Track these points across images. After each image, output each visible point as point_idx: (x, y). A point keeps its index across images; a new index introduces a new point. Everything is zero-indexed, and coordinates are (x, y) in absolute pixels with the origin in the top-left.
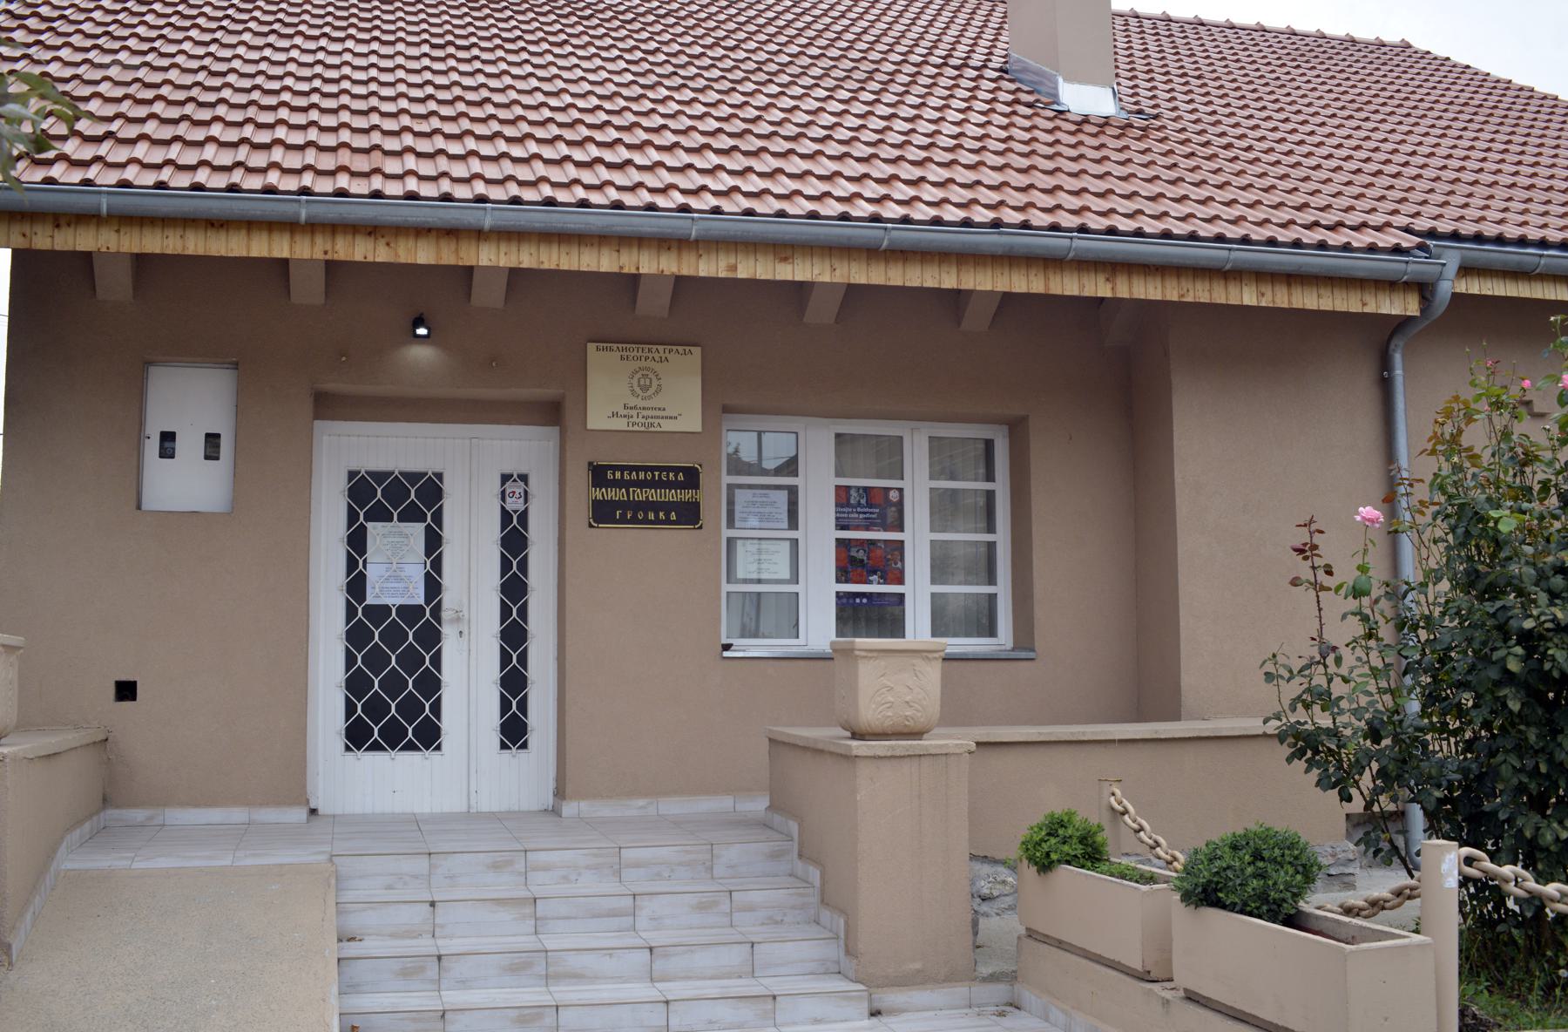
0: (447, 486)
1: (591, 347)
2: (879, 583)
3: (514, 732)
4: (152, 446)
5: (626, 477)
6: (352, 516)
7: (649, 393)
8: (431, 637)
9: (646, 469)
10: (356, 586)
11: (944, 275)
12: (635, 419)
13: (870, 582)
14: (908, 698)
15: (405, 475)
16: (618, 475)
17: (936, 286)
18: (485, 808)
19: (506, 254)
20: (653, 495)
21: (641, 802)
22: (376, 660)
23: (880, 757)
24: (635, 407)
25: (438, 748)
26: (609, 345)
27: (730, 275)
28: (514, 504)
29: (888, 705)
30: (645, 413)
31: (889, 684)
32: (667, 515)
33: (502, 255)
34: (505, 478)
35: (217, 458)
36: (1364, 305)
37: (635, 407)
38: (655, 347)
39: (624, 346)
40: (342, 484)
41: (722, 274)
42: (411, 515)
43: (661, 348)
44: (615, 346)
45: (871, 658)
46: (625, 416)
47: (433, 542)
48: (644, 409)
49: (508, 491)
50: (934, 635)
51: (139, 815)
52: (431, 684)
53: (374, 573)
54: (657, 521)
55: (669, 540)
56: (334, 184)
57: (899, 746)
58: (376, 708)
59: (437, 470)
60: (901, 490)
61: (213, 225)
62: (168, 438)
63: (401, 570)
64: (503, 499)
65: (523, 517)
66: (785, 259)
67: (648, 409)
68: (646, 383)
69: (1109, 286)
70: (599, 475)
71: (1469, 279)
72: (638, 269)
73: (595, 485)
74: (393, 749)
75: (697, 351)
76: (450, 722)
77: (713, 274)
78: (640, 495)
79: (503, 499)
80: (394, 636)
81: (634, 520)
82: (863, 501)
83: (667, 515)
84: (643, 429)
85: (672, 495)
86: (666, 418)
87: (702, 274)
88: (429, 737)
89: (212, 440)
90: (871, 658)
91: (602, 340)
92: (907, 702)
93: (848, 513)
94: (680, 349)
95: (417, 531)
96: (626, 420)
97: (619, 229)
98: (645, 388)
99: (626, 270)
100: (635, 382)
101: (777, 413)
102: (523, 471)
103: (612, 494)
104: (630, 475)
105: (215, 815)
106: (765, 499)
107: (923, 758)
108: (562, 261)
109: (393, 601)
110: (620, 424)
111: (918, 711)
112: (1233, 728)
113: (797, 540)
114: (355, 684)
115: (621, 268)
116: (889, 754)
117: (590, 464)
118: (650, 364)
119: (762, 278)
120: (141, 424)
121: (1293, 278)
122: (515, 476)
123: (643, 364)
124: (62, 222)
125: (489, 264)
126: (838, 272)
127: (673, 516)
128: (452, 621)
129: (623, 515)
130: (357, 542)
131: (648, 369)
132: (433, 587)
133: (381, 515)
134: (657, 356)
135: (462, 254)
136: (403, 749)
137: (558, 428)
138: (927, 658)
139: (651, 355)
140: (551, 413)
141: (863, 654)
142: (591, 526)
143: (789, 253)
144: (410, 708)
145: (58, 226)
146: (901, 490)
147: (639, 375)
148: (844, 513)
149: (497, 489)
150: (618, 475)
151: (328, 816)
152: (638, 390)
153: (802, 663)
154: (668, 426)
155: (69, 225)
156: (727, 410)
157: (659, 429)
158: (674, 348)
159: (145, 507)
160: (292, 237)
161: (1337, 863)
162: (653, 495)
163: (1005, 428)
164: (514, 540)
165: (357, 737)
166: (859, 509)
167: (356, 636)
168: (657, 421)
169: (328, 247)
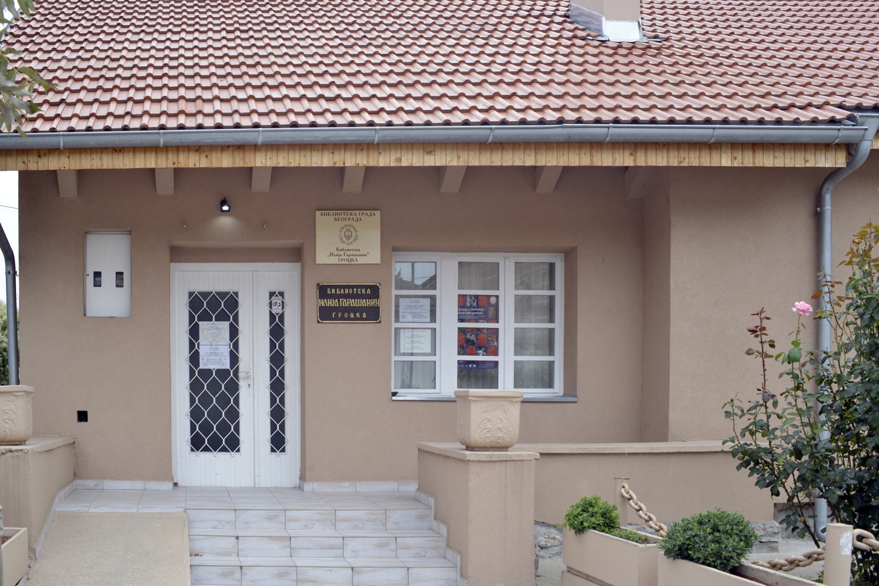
0: (240, 300)
1: (318, 213)
2: (483, 355)
3: (278, 442)
4: (90, 280)
5: (338, 292)
6: (191, 318)
8: (234, 387)
10: (194, 358)
11: (527, 158)
12: (343, 257)
13: (478, 354)
14: (500, 426)
15: (218, 293)
16: (333, 291)
17: (522, 164)
19: (270, 158)
20: (353, 303)
21: (347, 484)
22: (206, 400)
23: (483, 462)
24: (343, 250)
25: (238, 451)
26: (327, 212)
27: (398, 165)
28: (277, 310)
29: (488, 430)
30: (349, 253)
31: (489, 417)
32: (361, 315)
34: (272, 294)
35: (122, 286)
36: (806, 161)
37: (343, 250)
38: (354, 212)
40: (186, 300)
41: (393, 164)
42: (222, 317)
43: (357, 212)
44: (331, 212)
45: (479, 401)
46: (337, 255)
47: (234, 332)
48: (348, 250)
51: (91, 483)
52: (234, 415)
53: (203, 351)
54: (355, 319)
60: (497, 297)
61: (116, 150)
62: (97, 275)
63: (217, 349)
66: (430, 153)
67: (350, 250)
69: (632, 158)
70: (323, 291)
72: (344, 163)
75: (378, 213)
77: (387, 165)
78: (345, 303)
79: (271, 307)
81: (343, 318)
83: (361, 315)
84: (347, 263)
85: (364, 303)
86: (360, 255)
87: (381, 165)
88: (234, 444)
90: (479, 401)
92: (499, 428)
94: (368, 212)
95: (225, 326)
96: (337, 257)
99: (337, 165)
100: (342, 234)
102: (281, 290)
103: (331, 303)
104: (340, 291)
105: (127, 485)
107: (507, 462)
108: (301, 161)
110: (334, 260)
111: (505, 434)
112: (586, 449)
113: (435, 329)
114: (195, 414)
117: (318, 285)
118: (351, 222)
120: (84, 268)
121: (756, 146)
122: (277, 293)
123: (347, 223)
124: (42, 154)
125: (261, 165)
127: (364, 315)
128: (244, 378)
129: (337, 315)
130: (194, 333)
131: (349, 226)
132: (234, 359)
133: (206, 317)
134: (355, 218)
135: (247, 160)
136: (203, 450)
139: (351, 217)
141: (474, 399)
142: (319, 322)
143: (432, 148)
144: (224, 428)
145: (40, 156)
146: (497, 297)
149: (267, 301)
150: (333, 291)
154: (361, 260)
156: (395, 249)
157: (356, 262)
158: (365, 212)
159: (87, 315)
162: (353, 303)
163: (562, 255)
164: (277, 331)
165: (197, 444)
166: (472, 309)
167: (195, 387)
169: (175, 160)
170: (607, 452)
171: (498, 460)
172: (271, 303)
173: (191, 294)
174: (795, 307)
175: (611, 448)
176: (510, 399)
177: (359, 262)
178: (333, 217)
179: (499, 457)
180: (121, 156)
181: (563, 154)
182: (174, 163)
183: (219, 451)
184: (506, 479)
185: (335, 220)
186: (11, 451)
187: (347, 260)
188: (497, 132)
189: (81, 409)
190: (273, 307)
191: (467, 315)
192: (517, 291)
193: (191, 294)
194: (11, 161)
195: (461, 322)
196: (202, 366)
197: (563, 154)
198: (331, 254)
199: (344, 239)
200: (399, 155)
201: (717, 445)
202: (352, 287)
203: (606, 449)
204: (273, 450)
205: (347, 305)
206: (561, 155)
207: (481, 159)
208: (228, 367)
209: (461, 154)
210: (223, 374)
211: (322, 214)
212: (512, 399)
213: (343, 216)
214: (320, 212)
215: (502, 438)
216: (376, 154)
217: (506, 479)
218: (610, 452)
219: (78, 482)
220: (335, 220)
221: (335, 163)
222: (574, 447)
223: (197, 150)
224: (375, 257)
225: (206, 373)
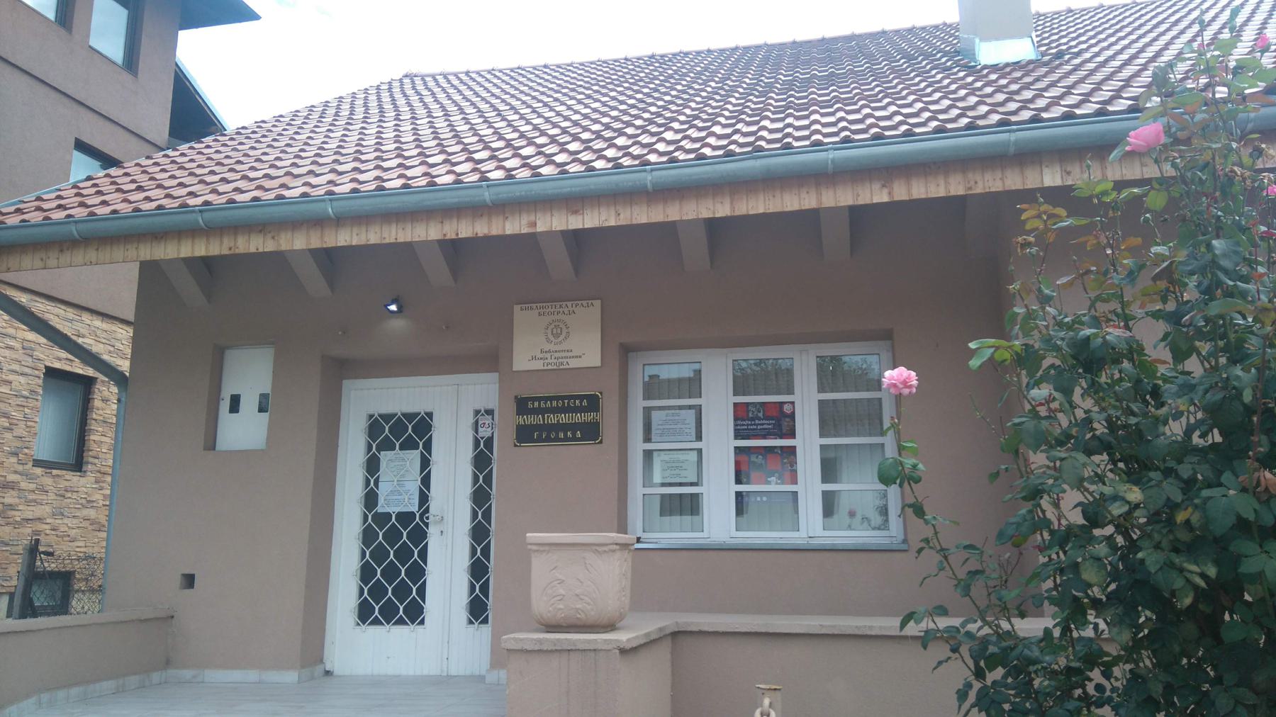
0: (436, 422)
1: (517, 308)
2: (777, 484)
3: (477, 610)
4: (225, 405)
5: (543, 405)
6: (370, 448)
7: (560, 339)
8: (419, 535)
10: (370, 499)
11: (719, 206)
12: (549, 361)
13: (769, 483)
14: (578, 591)
17: (711, 216)
19: (357, 235)
20: (564, 418)
22: (380, 555)
23: (527, 651)
24: (549, 351)
25: (422, 622)
26: (529, 305)
27: (531, 230)
29: (559, 598)
30: (557, 355)
31: (560, 577)
32: (574, 434)
33: (355, 236)
34: (477, 412)
37: (549, 351)
38: (564, 303)
39: (541, 304)
40: (363, 424)
41: (525, 230)
42: (409, 445)
43: (569, 304)
44: (534, 305)
45: (544, 551)
46: (541, 359)
47: (425, 463)
48: (556, 351)
49: (480, 422)
51: (187, 674)
52: (418, 573)
53: (383, 491)
54: (566, 439)
55: (582, 452)
56: (473, 229)
57: (547, 640)
60: (793, 403)
61: (156, 238)
63: (403, 486)
64: (477, 431)
66: (575, 212)
67: (559, 351)
68: (557, 331)
69: (885, 191)
70: (522, 405)
72: (457, 234)
74: (413, 623)
75: (598, 303)
77: (516, 231)
78: (553, 419)
79: (477, 431)
80: (393, 536)
81: (548, 439)
82: (761, 415)
83: (574, 434)
84: (555, 367)
85: (579, 418)
86: (573, 357)
87: (508, 232)
88: (415, 614)
90: (544, 551)
91: (526, 301)
92: (577, 595)
93: (748, 425)
94: (584, 303)
95: (414, 456)
96: (542, 361)
97: (429, 203)
98: (557, 336)
99: (448, 237)
100: (549, 331)
101: (689, 347)
102: (472, 414)
104: (545, 404)
105: (236, 675)
106: (677, 418)
107: (571, 653)
108: (399, 235)
109: (394, 509)
110: (538, 365)
111: (589, 604)
112: (834, 627)
113: (701, 449)
114: (366, 573)
115: (445, 235)
116: (537, 648)
117: (516, 397)
118: (560, 317)
119: (558, 229)
122: (483, 411)
123: (556, 317)
125: (345, 244)
126: (622, 216)
128: (436, 523)
129: (540, 436)
130: (372, 466)
131: (559, 321)
132: (424, 499)
133: (387, 445)
135: (326, 239)
136: (372, 623)
137: (496, 375)
138: (599, 552)
139: (561, 310)
141: (534, 548)
142: (516, 446)
145: (62, 251)
146: (793, 403)
147: (552, 326)
148: (743, 425)
149: (471, 420)
151: (340, 676)
152: (552, 338)
153: (685, 553)
154: (574, 364)
155: (68, 250)
157: (567, 367)
158: (580, 302)
160: (208, 240)
162: (564, 418)
165: (364, 614)
166: (757, 422)
167: (368, 536)
168: (565, 360)
169: (232, 244)
170: (873, 633)
171: (554, 648)
172: (477, 422)
174: (1021, 370)
175: (881, 628)
176: (594, 548)
177: (571, 366)
178: (537, 311)
179: (555, 645)
181: (774, 196)
182: (230, 249)
183: (393, 624)
184: (568, 682)
185: (540, 314)
187: (555, 364)
188: (654, 173)
189: (187, 571)
190: (480, 429)
191: (751, 429)
192: (822, 394)
193: (371, 416)
195: (701, 437)
196: (380, 509)
197: (774, 196)
198: (534, 358)
200: (532, 218)
201: (890, 624)
202: (562, 398)
203: (871, 628)
204: (471, 622)
205: (554, 422)
206: (771, 198)
207: (650, 214)
208: (415, 508)
209: (621, 211)
210: (405, 518)
211: (522, 309)
212: (597, 548)
213: (550, 309)
214: (520, 306)
215: (583, 611)
216: (501, 218)
217: (568, 682)
218: (879, 633)
219: (171, 672)
220: (540, 314)
221: (445, 235)
222: (812, 623)
223: (261, 231)
225: (383, 518)
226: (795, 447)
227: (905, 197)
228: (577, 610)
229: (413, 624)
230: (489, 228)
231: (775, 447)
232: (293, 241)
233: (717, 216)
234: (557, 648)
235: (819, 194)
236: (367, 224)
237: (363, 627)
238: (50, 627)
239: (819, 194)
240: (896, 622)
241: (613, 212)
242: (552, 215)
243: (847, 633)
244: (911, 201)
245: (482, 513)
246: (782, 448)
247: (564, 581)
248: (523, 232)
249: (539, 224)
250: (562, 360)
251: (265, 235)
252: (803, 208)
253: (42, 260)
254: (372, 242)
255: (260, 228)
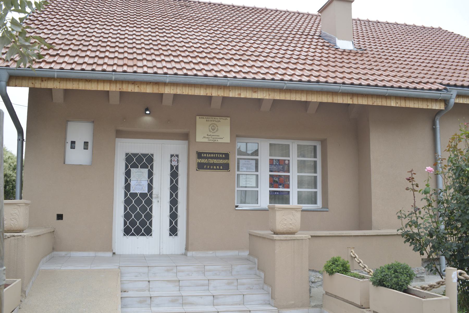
0: (155, 158)
1: (198, 117)
2: (282, 188)
3: (173, 231)
4: (69, 145)
5: (208, 156)
6: (127, 166)
7: (215, 131)
8: (149, 202)
9: (213, 153)
10: (128, 187)
11: (302, 97)
12: (210, 139)
13: (279, 188)
14: (291, 223)
16: (205, 155)
17: (300, 100)
18: (165, 253)
20: (215, 161)
21: (211, 252)
24: (210, 135)
25: (151, 235)
28: (174, 163)
29: (285, 224)
30: (213, 137)
31: (285, 218)
32: (220, 167)
33: (172, 90)
34: (172, 156)
35: (87, 149)
37: (210, 135)
38: (216, 117)
39: (207, 117)
40: (124, 157)
41: (237, 96)
42: (144, 166)
43: (218, 118)
45: (280, 210)
46: (207, 138)
47: (150, 174)
48: (213, 136)
49: (172, 160)
50: (298, 203)
51: (63, 253)
52: (149, 216)
53: (133, 183)
54: (217, 169)
58: (133, 223)
59: (152, 153)
60: (289, 160)
61: (87, 81)
62: (73, 143)
63: (141, 182)
64: (171, 162)
65: (177, 167)
66: (255, 92)
67: (214, 136)
68: (214, 128)
69: (351, 100)
70: (199, 155)
71: (459, 99)
72: (212, 94)
73: (198, 158)
75: (229, 119)
76: (155, 228)
77: (234, 96)
78: (211, 161)
79: (171, 162)
80: (138, 202)
81: (210, 169)
83: (220, 167)
84: (213, 142)
85: (221, 161)
86: (220, 138)
87: (231, 96)
88: (148, 232)
89: (86, 144)
90: (280, 210)
91: (200, 115)
93: (273, 167)
94: (224, 118)
95: (146, 171)
96: (208, 139)
98: (213, 130)
99: (208, 95)
100: (210, 128)
103: (203, 161)
104: (209, 155)
105: (85, 254)
106: (248, 163)
108: (189, 92)
110: (206, 140)
112: (333, 233)
114: (127, 216)
116: (285, 239)
117: (197, 152)
118: (215, 122)
121: (406, 98)
122: (175, 155)
123: (213, 122)
124: (44, 80)
125: (168, 93)
127: (221, 168)
129: (207, 167)
130: (128, 174)
131: (214, 124)
132: (150, 188)
133: (135, 166)
134: (217, 120)
135: (160, 90)
137: (188, 141)
138: (297, 211)
139: (215, 120)
140: (186, 137)
141: (278, 209)
142: (197, 170)
143: (256, 90)
144: (143, 223)
145: (42, 81)
146: (289, 160)
147: (212, 126)
149: (169, 159)
150: (205, 155)
151: (117, 255)
154: (220, 141)
156: (237, 136)
157: (217, 142)
158: (222, 118)
159: (66, 163)
161: (419, 273)
162: (215, 161)
163: (320, 142)
164: (174, 174)
165: (127, 232)
167: (127, 202)
168: (217, 139)
169: (121, 87)
172: (171, 160)
173: (127, 154)
175: (346, 233)
176: (296, 209)
177: (219, 142)
178: (206, 119)
179: (290, 238)
180: (90, 84)
182: (120, 89)
183: (140, 235)
186: (14, 236)
193: (127, 154)
194: (25, 82)
196: (131, 191)
199: (211, 130)
200: (240, 92)
204: (170, 235)
209: (270, 94)
210: (143, 195)
218: (345, 235)
221: (207, 94)
224: (227, 139)
226: (289, 176)
227: (356, 103)
228: (290, 228)
229: (128, 235)
230: (224, 93)
231: (282, 175)
232: (146, 89)
233: (302, 100)
234: (291, 239)
235: (333, 98)
236: (177, 86)
237: (128, 236)
238: (38, 235)
239: (333, 98)
240: (396, 231)
241: (268, 94)
242: (247, 92)
243: (337, 235)
244: (358, 104)
245: (175, 195)
246: (284, 176)
247: (286, 219)
248: (236, 97)
249: (242, 94)
250: (216, 139)
251: (135, 85)
252: (328, 102)
253: (33, 84)
254: (178, 93)
255: (133, 82)
